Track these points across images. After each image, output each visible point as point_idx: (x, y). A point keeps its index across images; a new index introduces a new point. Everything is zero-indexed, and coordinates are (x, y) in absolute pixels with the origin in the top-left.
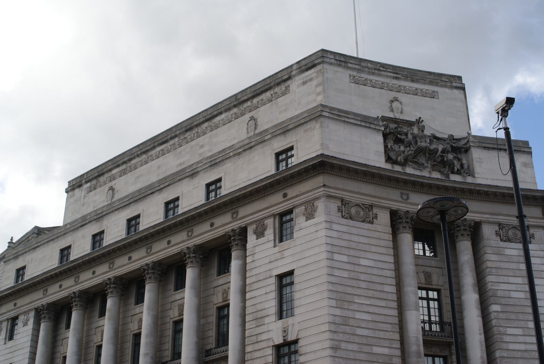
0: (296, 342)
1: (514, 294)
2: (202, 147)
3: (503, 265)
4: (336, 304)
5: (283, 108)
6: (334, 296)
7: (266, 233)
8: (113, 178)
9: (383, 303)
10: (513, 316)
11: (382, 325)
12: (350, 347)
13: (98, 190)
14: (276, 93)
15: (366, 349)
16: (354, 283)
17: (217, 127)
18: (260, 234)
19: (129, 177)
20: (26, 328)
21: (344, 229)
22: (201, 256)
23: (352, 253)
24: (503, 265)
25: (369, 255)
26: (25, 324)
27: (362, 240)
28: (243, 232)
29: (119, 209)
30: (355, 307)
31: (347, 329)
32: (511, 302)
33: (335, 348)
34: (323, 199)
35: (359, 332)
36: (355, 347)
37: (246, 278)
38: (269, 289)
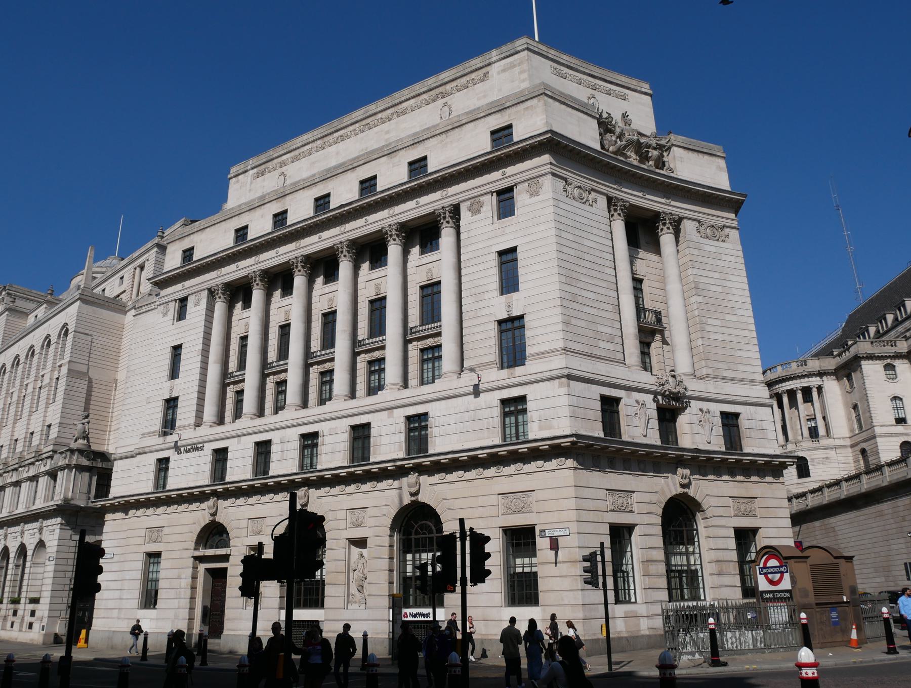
0: (521, 317)
1: (713, 288)
2: (387, 132)
3: (704, 260)
4: (566, 280)
5: (482, 94)
6: (563, 272)
7: (483, 210)
8: (284, 164)
10: (712, 308)
13: (267, 176)
14: (473, 79)
15: (593, 327)
17: (404, 113)
18: (475, 210)
19: (304, 163)
20: (198, 308)
21: (569, 208)
22: (403, 234)
23: (577, 232)
24: (704, 260)
25: (592, 237)
26: (197, 304)
28: (455, 211)
29: (304, 188)
32: (711, 294)
33: (566, 323)
34: (549, 176)
37: (461, 255)
38: (487, 265)
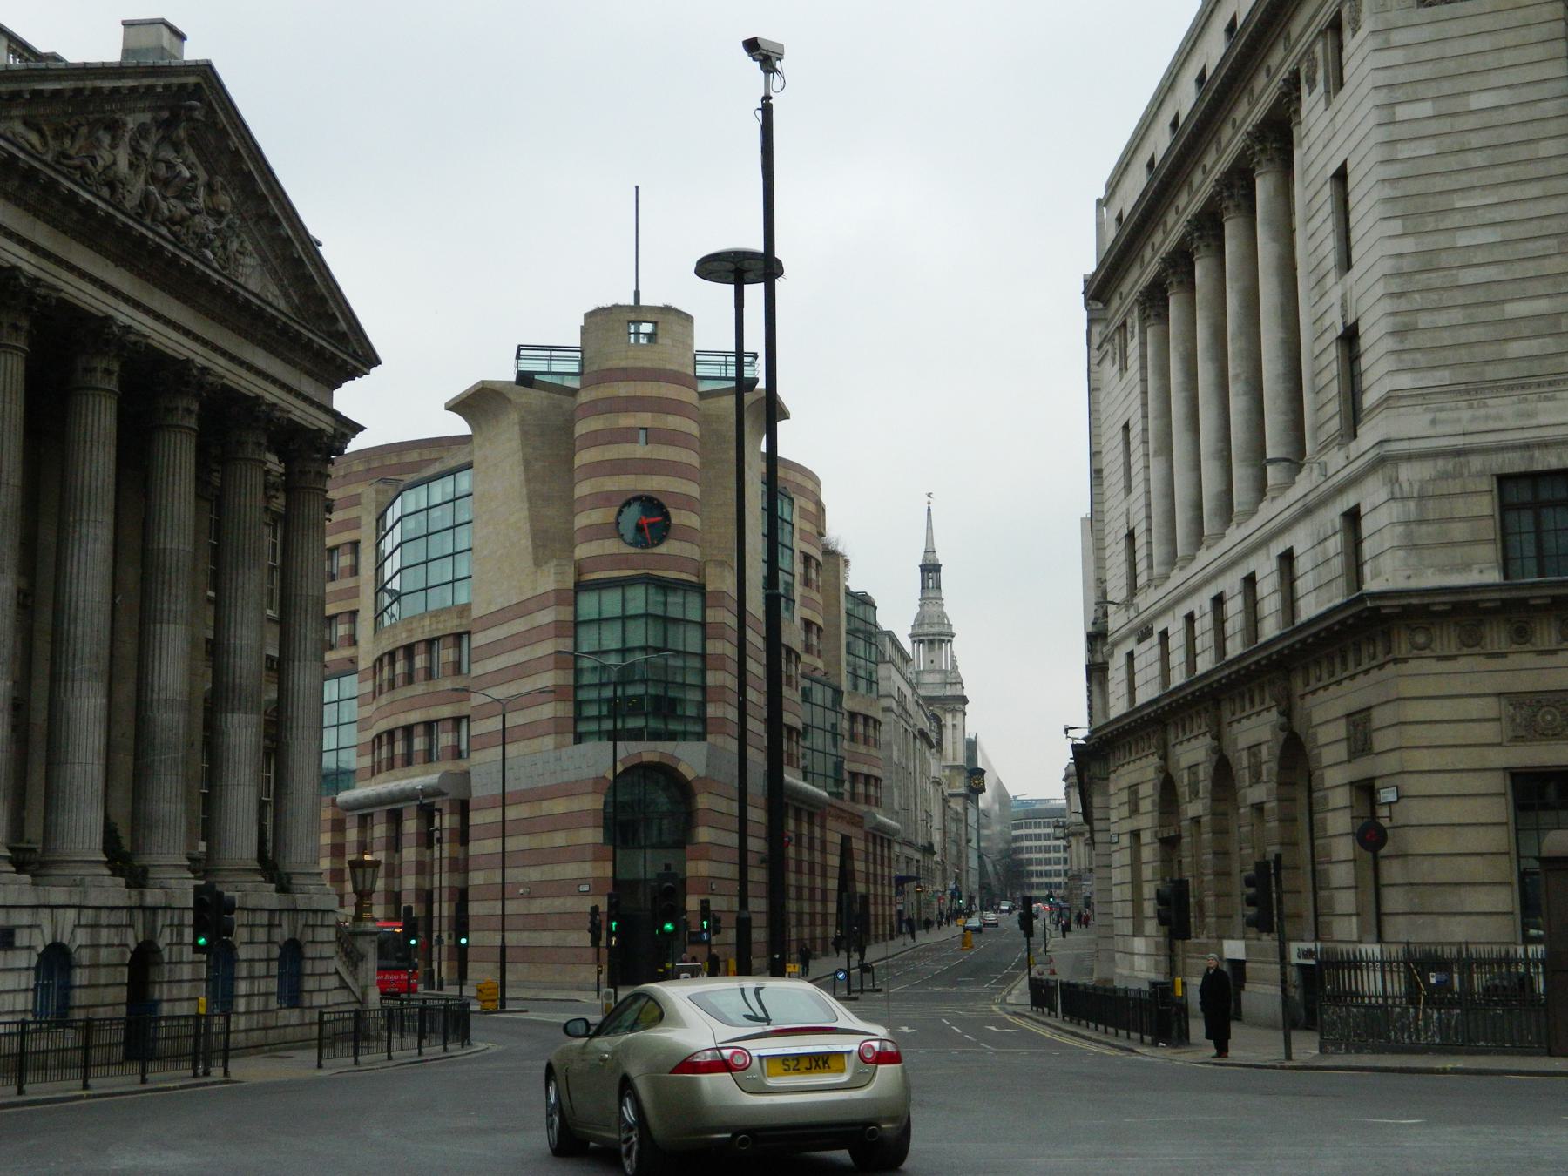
9: (1534, 190)
11: (1530, 245)
12: (1442, 319)
16: (1453, 162)
21: (1426, 33)
27: (1476, 44)
30: (1456, 220)
31: (1436, 279)
35: (1468, 276)
36: (1457, 316)
